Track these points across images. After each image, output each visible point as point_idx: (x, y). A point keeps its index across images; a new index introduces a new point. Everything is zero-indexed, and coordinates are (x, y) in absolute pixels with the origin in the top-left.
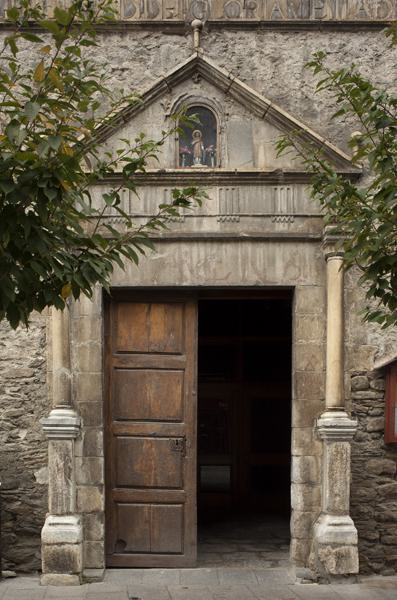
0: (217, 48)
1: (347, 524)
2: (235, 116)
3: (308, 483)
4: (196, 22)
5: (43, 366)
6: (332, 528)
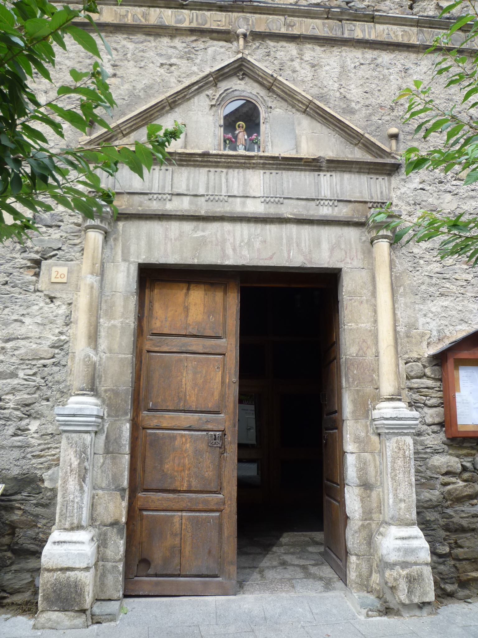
0: (261, 52)
1: (416, 538)
2: (278, 110)
3: (366, 486)
4: (241, 31)
5: (65, 346)
6: (400, 543)
